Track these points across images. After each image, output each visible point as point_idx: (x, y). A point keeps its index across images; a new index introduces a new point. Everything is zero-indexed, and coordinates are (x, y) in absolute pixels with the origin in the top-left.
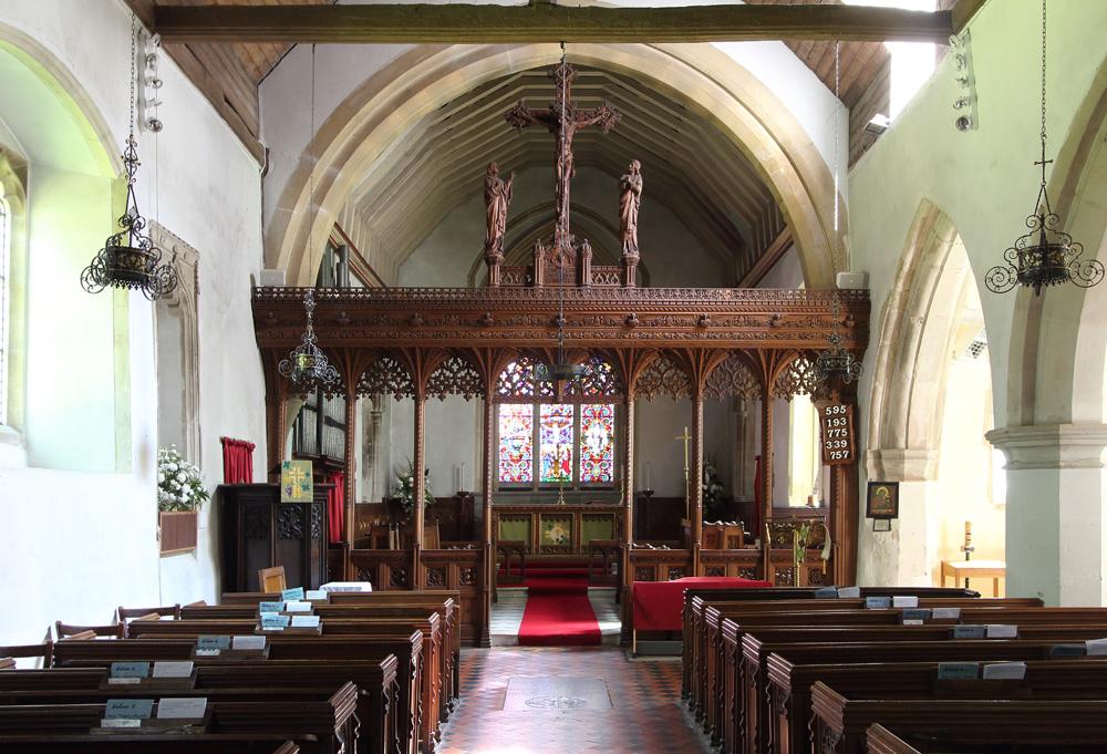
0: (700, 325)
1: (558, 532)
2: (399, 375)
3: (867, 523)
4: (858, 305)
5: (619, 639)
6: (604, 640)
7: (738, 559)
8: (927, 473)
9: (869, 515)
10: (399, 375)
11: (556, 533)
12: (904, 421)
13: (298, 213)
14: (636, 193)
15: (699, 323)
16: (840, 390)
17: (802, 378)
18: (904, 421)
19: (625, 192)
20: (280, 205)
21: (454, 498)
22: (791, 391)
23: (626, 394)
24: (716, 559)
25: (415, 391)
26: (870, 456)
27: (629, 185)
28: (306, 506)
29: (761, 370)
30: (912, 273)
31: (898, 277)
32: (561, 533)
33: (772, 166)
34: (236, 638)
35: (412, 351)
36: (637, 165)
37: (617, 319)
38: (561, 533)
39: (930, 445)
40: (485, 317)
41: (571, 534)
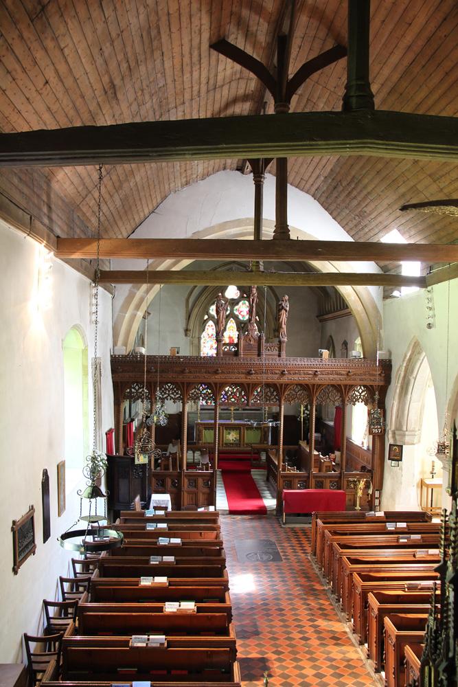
0: (315, 374)
1: (233, 435)
2: (175, 391)
3: (388, 462)
4: (387, 366)
5: (275, 513)
6: (268, 512)
7: (330, 477)
8: (415, 441)
9: (389, 459)
10: (175, 391)
11: (232, 436)
12: (406, 419)
13: (128, 316)
14: (286, 311)
15: (315, 374)
16: (378, 397)
17: (360, 395)
18: (406, 419)
19: (282, 309)
20: (120, 312)
21: (177, 414)
22: (356, 401)
23: (280, 402)
24: (320, 477)
25: (183, 399)
26: (390, 432)
27: (283, 307)
28: (144, 465)
29: (343, 392)
30: (410, 359)
31: (404, 361)
32: (235, 436)
33: (348, 296)
34: (164, 557)
35: (183, 383)
36: (287, 297)
37: (277, 372)
38: (235, 436)
39: (417, 429)
40: (218, 370)
41: (240, 437)
